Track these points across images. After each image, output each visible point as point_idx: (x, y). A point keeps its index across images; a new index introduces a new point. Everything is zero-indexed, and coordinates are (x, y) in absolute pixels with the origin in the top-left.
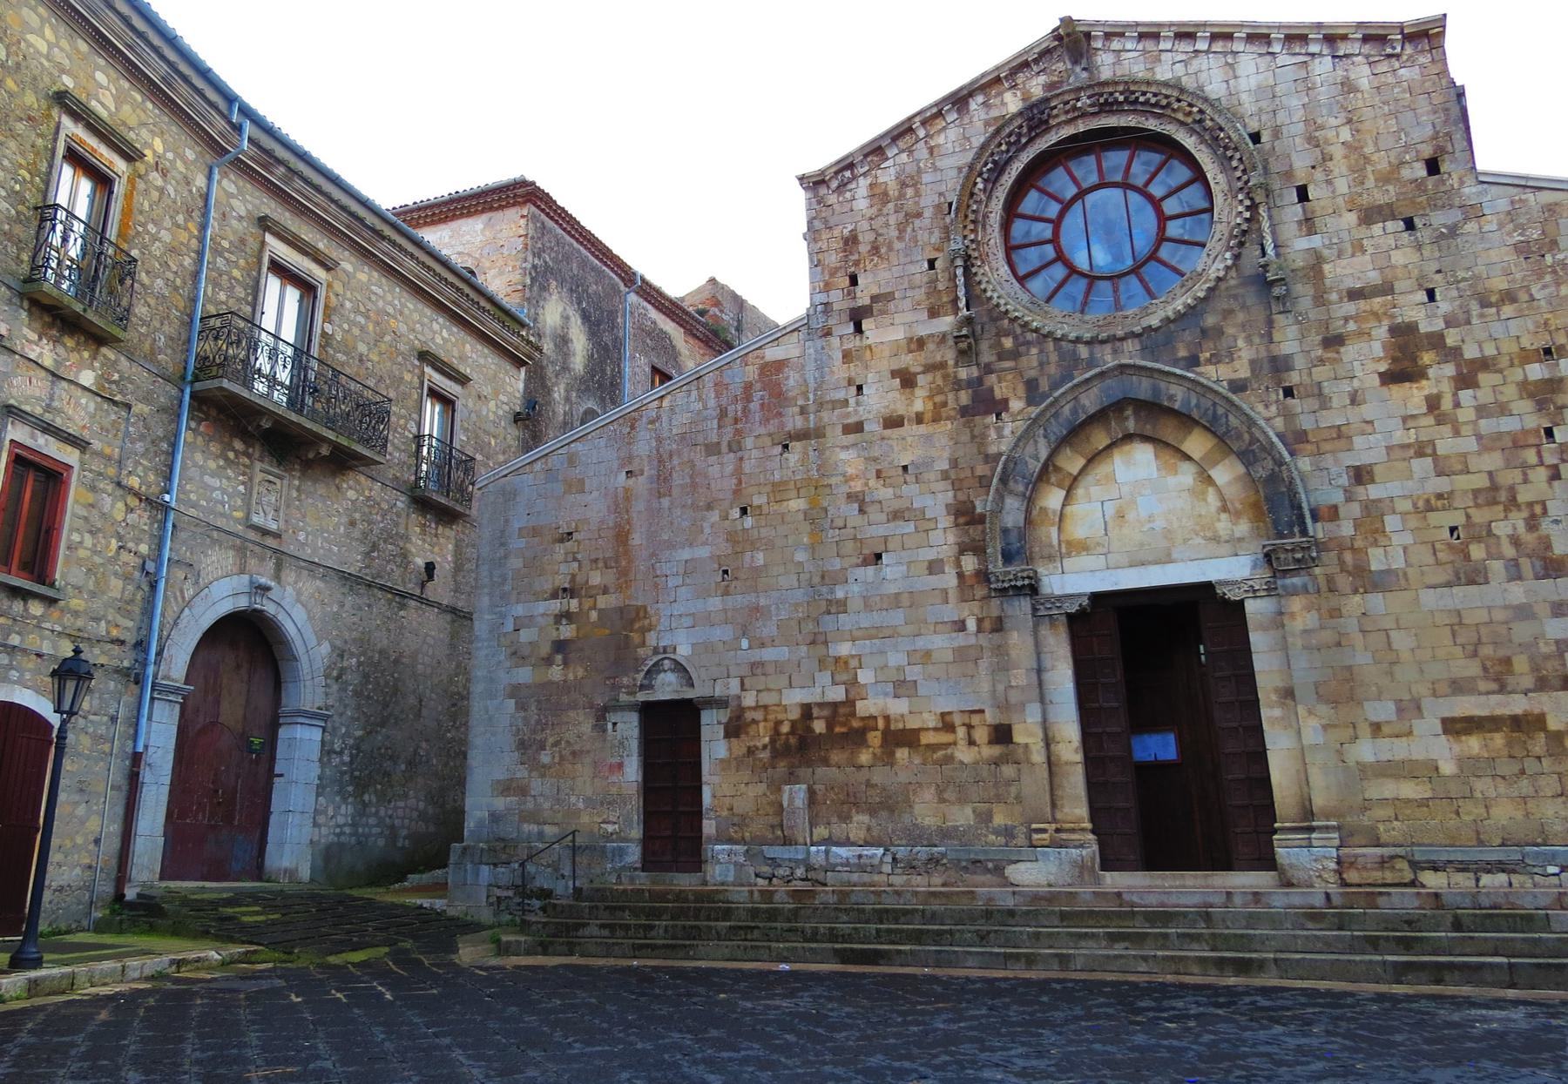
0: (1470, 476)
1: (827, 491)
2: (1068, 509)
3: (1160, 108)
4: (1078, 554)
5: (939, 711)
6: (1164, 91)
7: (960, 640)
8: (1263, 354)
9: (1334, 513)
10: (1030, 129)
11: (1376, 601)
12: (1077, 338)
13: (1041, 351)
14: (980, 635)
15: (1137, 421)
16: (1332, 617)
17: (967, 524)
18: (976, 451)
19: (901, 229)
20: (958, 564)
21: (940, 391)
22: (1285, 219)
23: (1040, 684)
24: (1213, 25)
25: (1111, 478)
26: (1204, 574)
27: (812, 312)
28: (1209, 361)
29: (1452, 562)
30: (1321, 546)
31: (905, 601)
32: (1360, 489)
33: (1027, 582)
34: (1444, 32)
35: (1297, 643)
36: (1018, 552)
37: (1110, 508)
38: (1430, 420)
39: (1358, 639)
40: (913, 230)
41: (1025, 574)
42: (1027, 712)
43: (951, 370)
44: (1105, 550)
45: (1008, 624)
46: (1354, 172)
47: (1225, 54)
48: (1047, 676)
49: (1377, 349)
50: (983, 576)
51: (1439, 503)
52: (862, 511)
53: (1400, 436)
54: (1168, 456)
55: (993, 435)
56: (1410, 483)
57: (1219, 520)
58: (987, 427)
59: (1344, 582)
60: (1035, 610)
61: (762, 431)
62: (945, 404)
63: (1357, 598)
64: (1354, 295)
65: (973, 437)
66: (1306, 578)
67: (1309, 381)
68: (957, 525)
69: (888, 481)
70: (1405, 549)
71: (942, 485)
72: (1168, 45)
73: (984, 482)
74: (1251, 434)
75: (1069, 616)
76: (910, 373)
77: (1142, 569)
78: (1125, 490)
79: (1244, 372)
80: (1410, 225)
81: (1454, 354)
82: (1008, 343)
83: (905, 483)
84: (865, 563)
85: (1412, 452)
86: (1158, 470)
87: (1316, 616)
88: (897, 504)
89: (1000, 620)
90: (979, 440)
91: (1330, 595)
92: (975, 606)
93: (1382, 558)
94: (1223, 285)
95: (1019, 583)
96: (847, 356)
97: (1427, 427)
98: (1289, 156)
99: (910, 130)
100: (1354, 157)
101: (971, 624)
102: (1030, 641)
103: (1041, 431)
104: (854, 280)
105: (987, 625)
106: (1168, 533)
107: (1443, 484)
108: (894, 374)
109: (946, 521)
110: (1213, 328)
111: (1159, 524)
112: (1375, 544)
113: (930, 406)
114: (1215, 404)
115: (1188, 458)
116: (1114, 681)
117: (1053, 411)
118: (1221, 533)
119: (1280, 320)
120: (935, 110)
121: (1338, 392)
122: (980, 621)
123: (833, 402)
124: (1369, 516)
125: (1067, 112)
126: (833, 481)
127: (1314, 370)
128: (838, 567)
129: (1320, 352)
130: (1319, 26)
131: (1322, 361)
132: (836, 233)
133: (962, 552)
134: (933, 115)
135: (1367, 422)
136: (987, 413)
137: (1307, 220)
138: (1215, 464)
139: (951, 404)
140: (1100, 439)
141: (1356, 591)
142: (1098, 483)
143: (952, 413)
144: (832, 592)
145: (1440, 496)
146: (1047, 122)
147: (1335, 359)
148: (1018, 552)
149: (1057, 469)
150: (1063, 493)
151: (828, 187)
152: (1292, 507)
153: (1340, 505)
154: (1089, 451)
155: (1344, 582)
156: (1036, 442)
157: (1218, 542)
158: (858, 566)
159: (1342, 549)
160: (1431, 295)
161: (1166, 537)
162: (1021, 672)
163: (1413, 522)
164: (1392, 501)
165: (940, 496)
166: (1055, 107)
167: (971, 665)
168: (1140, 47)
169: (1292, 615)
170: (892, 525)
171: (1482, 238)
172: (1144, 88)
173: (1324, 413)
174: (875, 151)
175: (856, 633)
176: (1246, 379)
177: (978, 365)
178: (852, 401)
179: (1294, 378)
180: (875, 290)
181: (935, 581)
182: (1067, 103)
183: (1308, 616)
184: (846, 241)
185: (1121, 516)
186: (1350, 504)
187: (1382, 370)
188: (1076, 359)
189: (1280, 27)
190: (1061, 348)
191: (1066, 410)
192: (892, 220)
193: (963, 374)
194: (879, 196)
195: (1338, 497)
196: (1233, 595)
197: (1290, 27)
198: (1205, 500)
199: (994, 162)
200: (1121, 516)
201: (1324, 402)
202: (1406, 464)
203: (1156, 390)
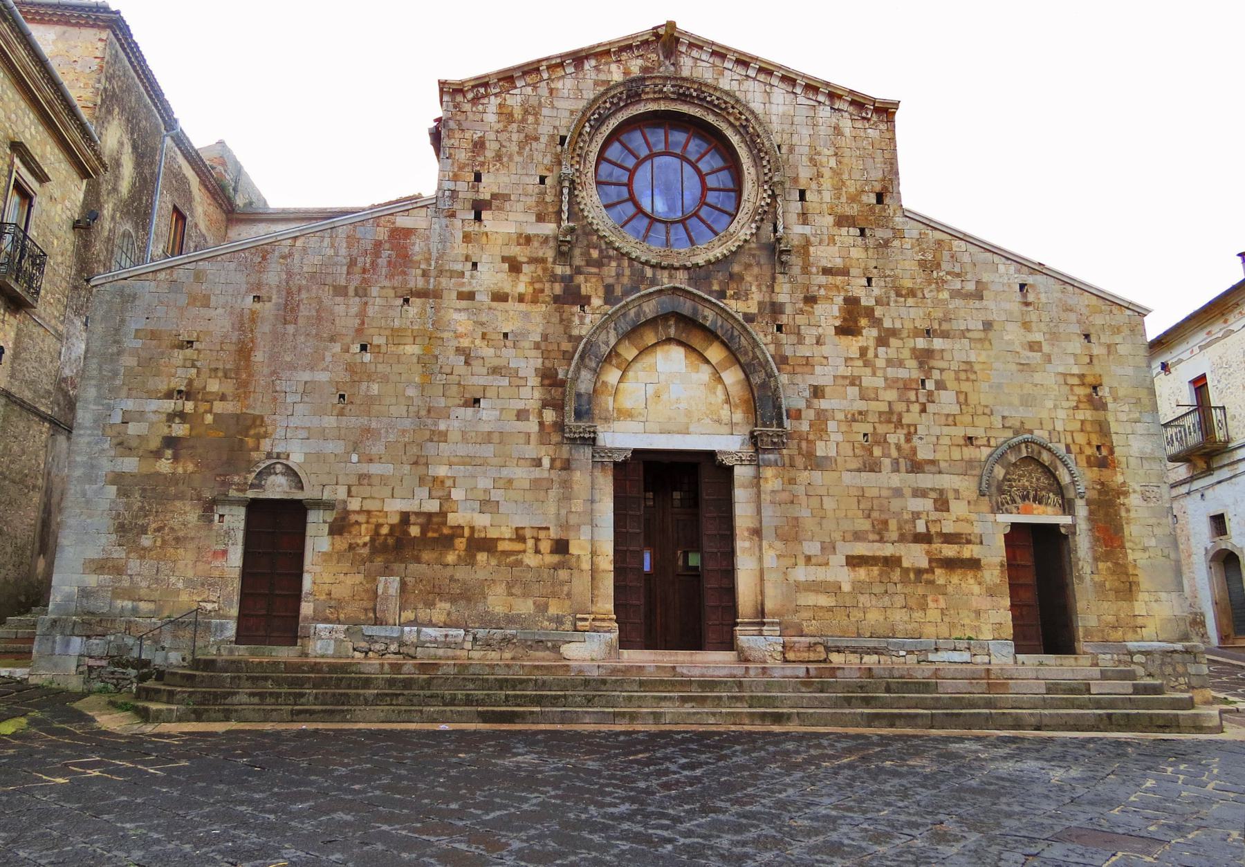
1: (440, 342)
4: (625, 419)
5: (514, 526)
7: (536, 473)
8: (767, 299)
9: (798, 415)
10: (628, 97)
11: (817, 475)
14: (552, 471)
20: (540, 414)
21: (540, 280)
25: (653, 368)
27: (440, 194)
31: (496, 438)
32: (816, 401)
35: (766, 497)
37: (651, 389)
38: (860, 363)
39: (803, 499)
44: (644, 419)
54: (694, 357)
55: (576, 320)
58: (573, 314)
59: (800, 461)
62: (542, 291)
63: (807, 473)
65: (561, 320)
70: (837, 444)
74: (754, 353)
84: (466, 404)
85: (848, 382)
90: (566, 323)
91: (791, 469)
95: (587, 436)
97: (858, 369)
99: (538, 70)
101: (546, 462)
105: (558, 464)
106: (688, 413)
109: (534, 381)
111: (683, 405)
113: (530, 290)
115: (707, 361)
120: (559, 60)
121: (810, 334)
122: (553, 460)
123: (451, 271)
129: (802, 305)
131: (802, 312)
133: (545, 404)
137: (803, 214)
139: (547, 292)
140: (650, 338)
141: (806, 469)
142: (644, 370)
143: (547, 299)
145: (860, 413)
151: (464, 97)
152: (774, 407)
154: (642, 346)
156: (608, 332)
159: (801, 440)
163: (844, 428)
167: (542, 493)
168: (711, 60)
169: (766, 479)
170: (490, 378)
174: (508, 78)
178: (467, 274)
179: (784, 319)
181: (521, 426)
190: (633, 265)
191: (632, 313)
195: (802, 404)
198: (715, 393)
203: (695, 310)
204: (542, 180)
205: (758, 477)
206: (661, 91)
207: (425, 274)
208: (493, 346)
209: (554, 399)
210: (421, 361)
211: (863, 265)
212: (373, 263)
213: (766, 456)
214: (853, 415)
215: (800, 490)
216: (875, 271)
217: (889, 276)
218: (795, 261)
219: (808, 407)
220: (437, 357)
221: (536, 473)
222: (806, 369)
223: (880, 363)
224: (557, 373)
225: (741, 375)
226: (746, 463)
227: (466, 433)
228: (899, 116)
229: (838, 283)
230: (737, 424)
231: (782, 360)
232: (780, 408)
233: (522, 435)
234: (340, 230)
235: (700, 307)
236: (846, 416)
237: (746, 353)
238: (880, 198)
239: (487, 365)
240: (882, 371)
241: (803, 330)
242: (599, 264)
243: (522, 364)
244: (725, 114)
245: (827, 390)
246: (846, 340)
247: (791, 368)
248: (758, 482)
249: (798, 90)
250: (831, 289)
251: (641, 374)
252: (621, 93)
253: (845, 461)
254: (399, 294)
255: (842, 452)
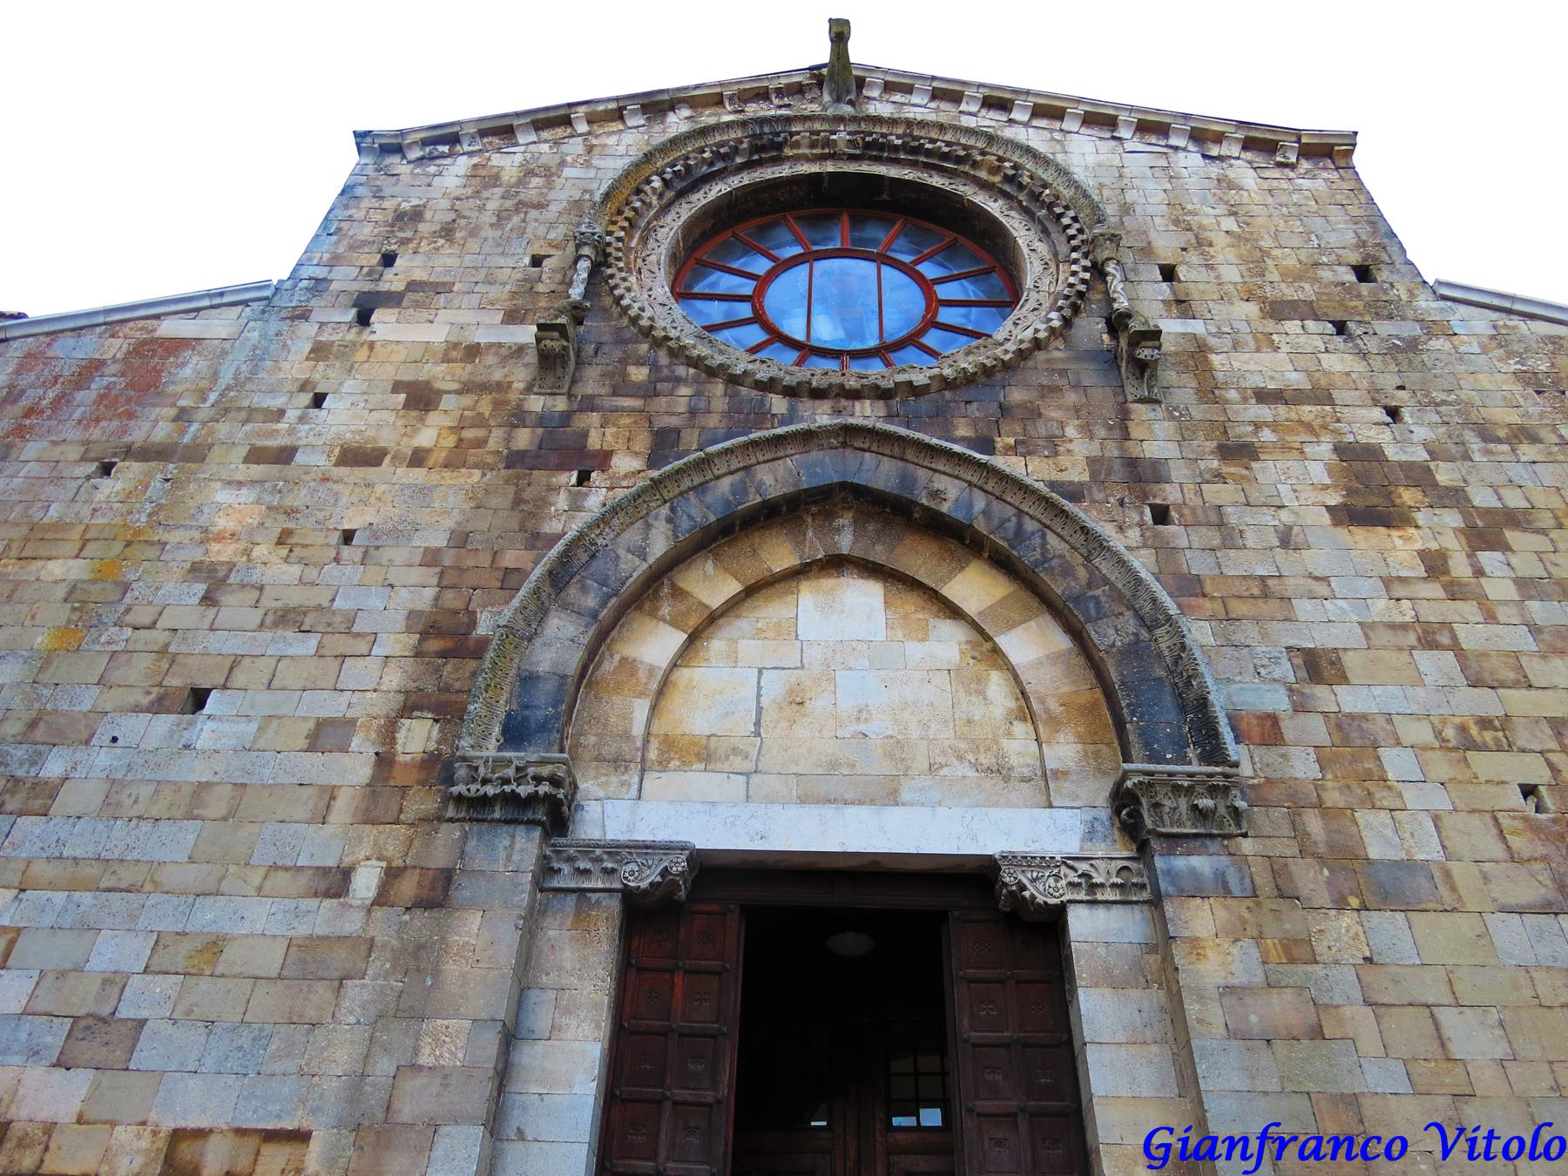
0: (1533, 692)
1: (152, 553)
2: (683, 675)
3: (955, 161)
4: (685, 765)
5: (168, 1124)
6: (963, 141)
7: (321, 918)
8: (1112, 451)
9: (1270, 731)
10: (755, 149)
11: (1389, 928)
12: (772, 379)
13: (698, 394)
14: (379, 913)
15: (856, 539)
16: (1292, 960)
17: (444, 654)
18: (515, 525)
19: (501, 218)
20: (389, 732)
21: (480, 422)
22: (1141, 295)
23: (503, 1074)
24: (1038, 94)
25: (789, 631)
26: (974, 839)
27: (288, 285)
28: (1012, 450)
29: (1544, 859)
30: (1259, 795)
31: (216, 805)
32: (1320, 691)
33: (544, 788)
34: (1352, 151)
35: (1207, 1017)
36: (543, 728)
37: (775, 685)
38: (1435, 590)
39: (1360, 1019)
40: (524, 221)
41: (545, 771)
42: (439, 1151)
43: (513, 396)
44: (748, 766)
45: (464, 890)
46: (1247, 262)
47: (1051, 131)
48: (529, 1055)
49: (1318, 472)
50: (438, 768)
51: (1488, 736)
52: (208, 600)
53: (1380, 608)
54: (910, 604)
55: (561, 501)
56: (1420, 692)
57: (1009, 735)
58: (557, 489)
59: (1311, 879)
60: (545, 870)
61: (75, 434)
62: (481, 443)
63: (1347, 920)
64: (1262, 396)
65: (518, 501)
66: (1224, 861)
67: (1197, 502)
68: (418, 654)
69: (298, 551)
70: (1436, 820)
71: (417, 574)
72: (974, 108)
73: (510, 579)
74: (1093, 571)
75: (628, 895)
76: (431, 389)
77: (828, 811)
78: (814, 655)
79: (1077, 474)
80: (1341, 328)
81: (1454, 497)
82: (639, 374)
83: (337, 560)
84: (159, 706)
85: (1411, 639)
86: (889, 626)
87: (1255, 953)
88: (297, 597)
89: (447, 877)
90: (528, 512)
91: (1282, 904)
92: (393, 840)
93: (1389, 833)
94: (1040, 356)
95: (524, 790)
96: (319, 351)
97: (1431, 602)
98: (1145, 233)
99: (566, 121)
100: (1244, 250)
101: (366, 882)
102: (509, 938)
103: (665, 511)
104: (388, 260)
105: (408, 888)
106: (897, 748)
107: (1486, 702)
108: (397, 387)
109: (396, 642)
110: (1023, 406)
111: (879, 726)
112: (1370, 802)
113: (450, 441)
114: (1020, 513)
115: (953, 611)
116: (709, 1096)
117: (697, 480)
118: (1014, 761)
119: (1140, 411)
120: (613, 106)
121: (1258, 527)
122: (392, 875)
123: (251, 410)
124: (1346, 742)
125: (813, 145)
126: (173, 537)
127: (1204, 487)
128: (87, 706)
129: (1215, 464)
130: (1186, 117)
131: (1219, 477)
132: (387, 204)
133: (410, 706)
134: (614, 112)
135: (1316, 578)
136: (563, 467)
137: (1179, 302)
138: (1010, 625)
139: (492, 444)
140: (779, 554)
141: (1341, 905)
142: (759, 634)
143: (490, 459)
144: (37, 760)
145: (1485, 723)
146: (779, 147)
147: (1243, 477)
148: (543, 728)
149: (678, 593)
150: (679, 638)
151: (404, 157)
152: (1183, 709)
153: (1282, 716)
154: (753, 574)
155: (1311, 879)
156: (648, 526)
157: (1007, 779)
158: (137, 709)
159: (1296, 808)
160: (1393, 413)
161: (891, 756)
162: (459, 1025)
163: (1441, 766)
164: (1390, 721)
165: (404, 592)
166: (798, 133)
167: (323, 991)
168: (933, 105)
169: (1195, 943)
170: (267, 635)
171: (1461, 359)
172: (934, 135)
173: (1232, 553)
174: (501, 130)
175: (42, 869)
176: (1081, 484)
177: (570, 396)
178: (292, 415)
179: (1170, 494)
180: (420, 275)
181: (318, 767)
182: (818, 133)
183: (1235, 950)
184: (400, 216)
185: (797, 701)
186: (1302, 717)
187: (1333, 503)
188: (762, 416)
189: (1132, 109)
190: (737, 394)
191: (725, 485)
192: (492, 205)
193: (536, 404)
194: (483, 179)
195: (1276, 701)
196: (1043, 891)
197: (1146, 111)
198: (981, 693)
199: (688, 168)
200: (797, 701)
201: (1230, 538)
202: (1405, 656)
203: (907, 480)
204: (537, 261)
205: (1163, 942)
206: (828, 143)
207: (183, 416)
208: (300, 561)
209: (446, 689)
210: (78, 595)
211: (1365, 384)
212: (57, 401)
213: (1180, 862)
214: (1463, 729)
215: (1343, 984)
216: (1401, 393)
217: (1444, 403)
218: (1181, 388)
219: (1300, 708)
220: (126, 587)
221: (321, 918)
222: (1263, 607)
223: (1499, 588)
224: (473, 624)
225: (1062, 642)
226: (1110, 895)
227: (123, 784)
228: (1358, 159)
229: (1307, 418)
230: (1060, 774)
231: (1189, 587)
232: (1203, 703)
233: (307, 792)
234: (15, 344)
235: (921, 473)
236: (1438, 734)
237: (1067, 571)
238: (1363, 273)
239: (267, 603)
240: (1513, 610)
241: (1233, 516)
242: (648, 391)
243: (375, 601)
244: (967, 168)
245: (1349, 660)
246: (1364, 539)
247: (1218, 606)
248: (1168, 958)
249: (1124, 133)
250: (1292, 431)
251: (747, 648)
252: (740, 141)
253: (1486, 878)
254: (92, 455)
255: (1458, 844)
